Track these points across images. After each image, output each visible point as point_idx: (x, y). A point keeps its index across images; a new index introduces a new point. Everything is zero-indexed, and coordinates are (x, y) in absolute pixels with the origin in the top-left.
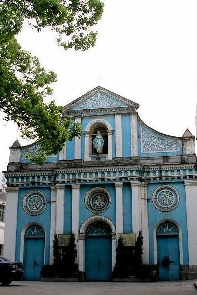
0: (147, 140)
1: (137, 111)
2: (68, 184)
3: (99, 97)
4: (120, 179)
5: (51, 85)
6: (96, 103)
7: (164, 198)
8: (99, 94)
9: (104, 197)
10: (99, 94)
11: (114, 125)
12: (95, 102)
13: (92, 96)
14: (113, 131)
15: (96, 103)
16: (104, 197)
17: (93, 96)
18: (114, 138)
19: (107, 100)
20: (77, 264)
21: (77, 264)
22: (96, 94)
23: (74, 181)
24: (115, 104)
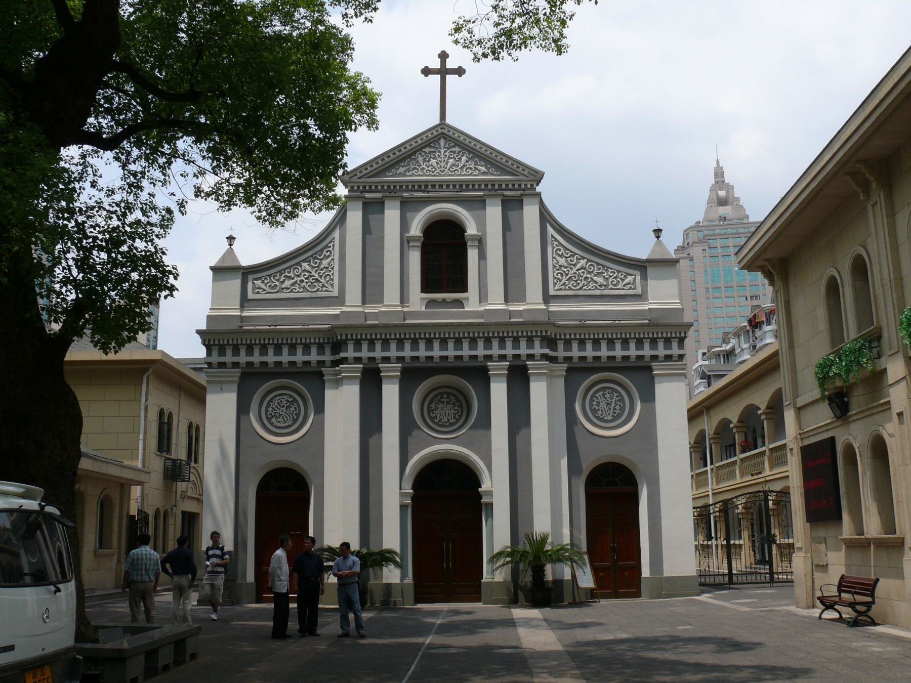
0: (562, 261)
1: (538, 189)
2: (372, 365)
3: (442, 152)
4: (502, 358)
5: (491, 57)
6: (435, 165)
7: (603, 405)
8: (442, 142)
9: (458, 400)
10: (442, 142)
11: (481, 224)
12: (433, 161)
13: (425, 147)
14: (481, 242)
15: (435, 165)
16: (458, 400)
17: (429, 145)
18: (482, 256)
19: (464, 158)
20: (807, 522)
21: (807, 522)
22: (439, 139)
23: (386, 360)
24: (479, 173)
